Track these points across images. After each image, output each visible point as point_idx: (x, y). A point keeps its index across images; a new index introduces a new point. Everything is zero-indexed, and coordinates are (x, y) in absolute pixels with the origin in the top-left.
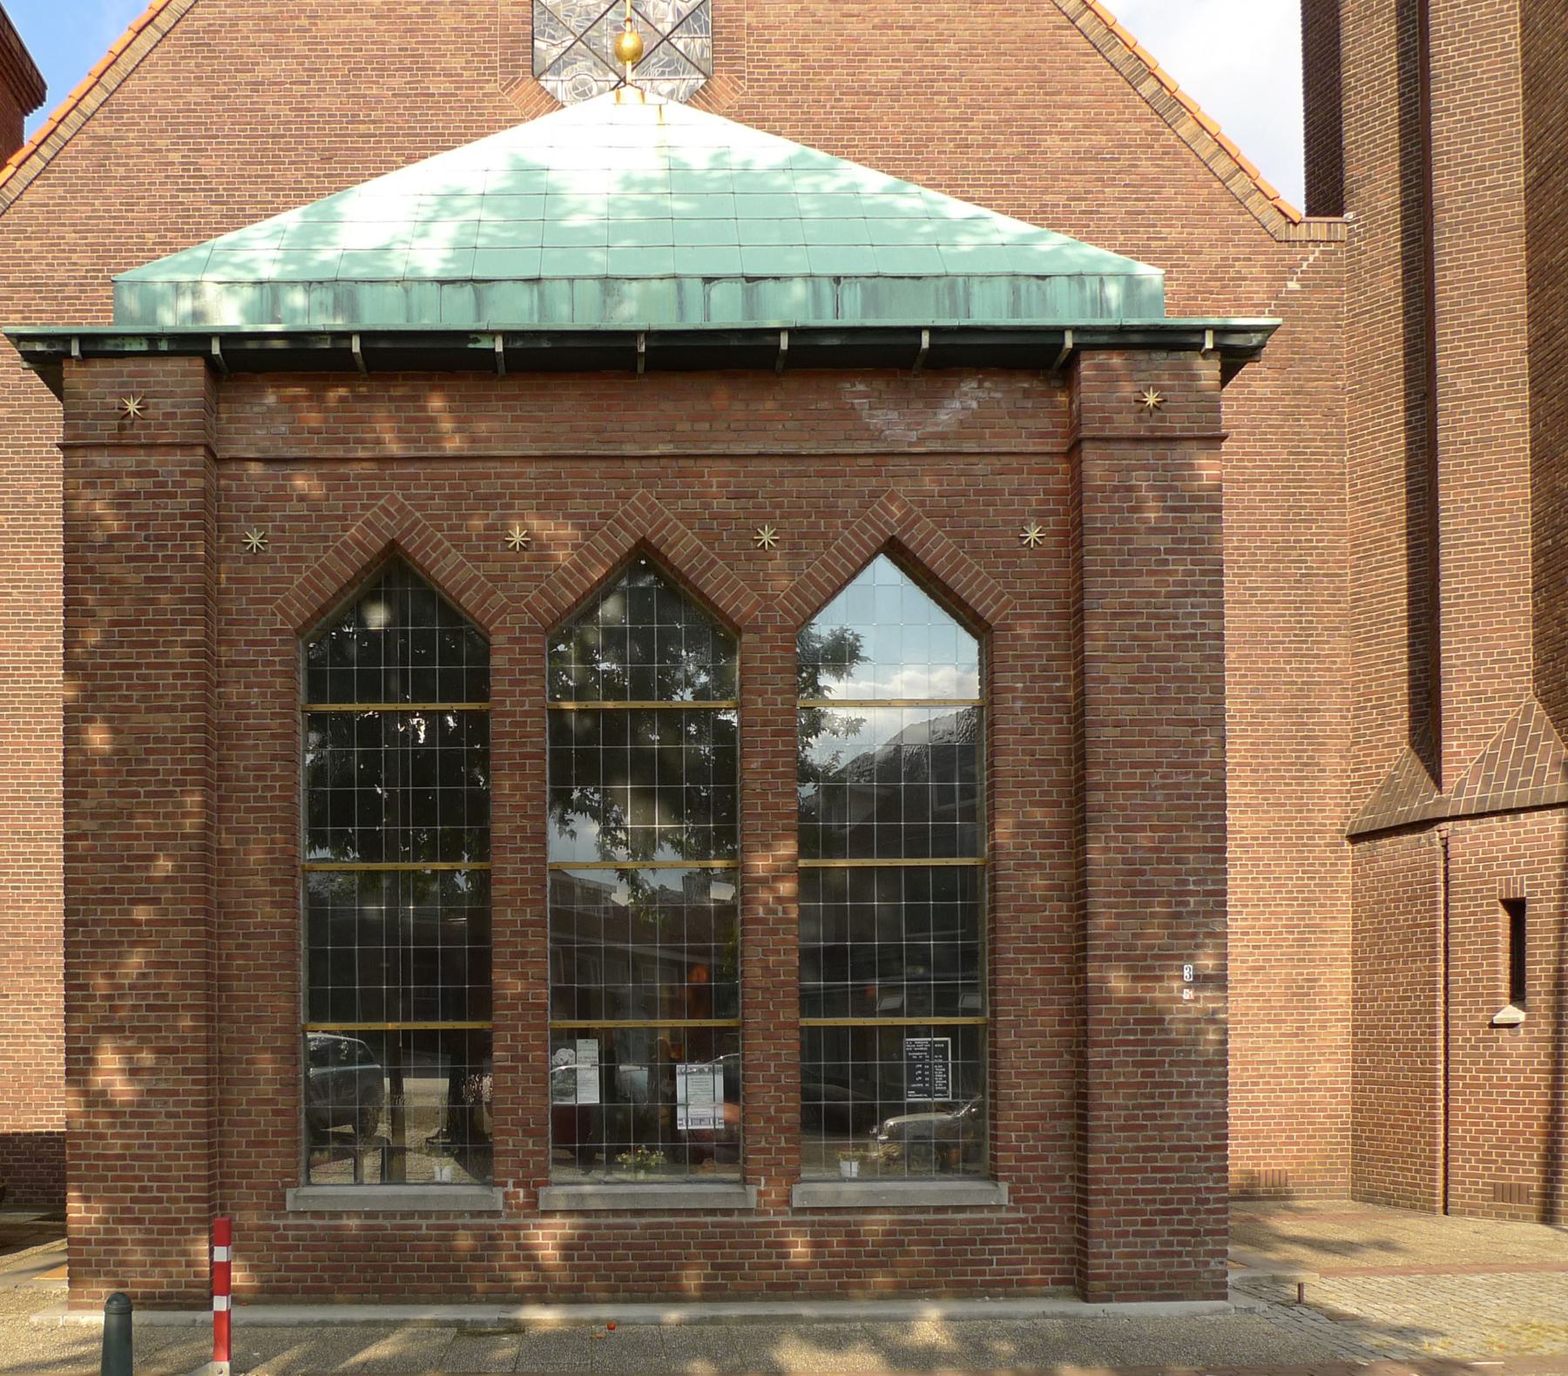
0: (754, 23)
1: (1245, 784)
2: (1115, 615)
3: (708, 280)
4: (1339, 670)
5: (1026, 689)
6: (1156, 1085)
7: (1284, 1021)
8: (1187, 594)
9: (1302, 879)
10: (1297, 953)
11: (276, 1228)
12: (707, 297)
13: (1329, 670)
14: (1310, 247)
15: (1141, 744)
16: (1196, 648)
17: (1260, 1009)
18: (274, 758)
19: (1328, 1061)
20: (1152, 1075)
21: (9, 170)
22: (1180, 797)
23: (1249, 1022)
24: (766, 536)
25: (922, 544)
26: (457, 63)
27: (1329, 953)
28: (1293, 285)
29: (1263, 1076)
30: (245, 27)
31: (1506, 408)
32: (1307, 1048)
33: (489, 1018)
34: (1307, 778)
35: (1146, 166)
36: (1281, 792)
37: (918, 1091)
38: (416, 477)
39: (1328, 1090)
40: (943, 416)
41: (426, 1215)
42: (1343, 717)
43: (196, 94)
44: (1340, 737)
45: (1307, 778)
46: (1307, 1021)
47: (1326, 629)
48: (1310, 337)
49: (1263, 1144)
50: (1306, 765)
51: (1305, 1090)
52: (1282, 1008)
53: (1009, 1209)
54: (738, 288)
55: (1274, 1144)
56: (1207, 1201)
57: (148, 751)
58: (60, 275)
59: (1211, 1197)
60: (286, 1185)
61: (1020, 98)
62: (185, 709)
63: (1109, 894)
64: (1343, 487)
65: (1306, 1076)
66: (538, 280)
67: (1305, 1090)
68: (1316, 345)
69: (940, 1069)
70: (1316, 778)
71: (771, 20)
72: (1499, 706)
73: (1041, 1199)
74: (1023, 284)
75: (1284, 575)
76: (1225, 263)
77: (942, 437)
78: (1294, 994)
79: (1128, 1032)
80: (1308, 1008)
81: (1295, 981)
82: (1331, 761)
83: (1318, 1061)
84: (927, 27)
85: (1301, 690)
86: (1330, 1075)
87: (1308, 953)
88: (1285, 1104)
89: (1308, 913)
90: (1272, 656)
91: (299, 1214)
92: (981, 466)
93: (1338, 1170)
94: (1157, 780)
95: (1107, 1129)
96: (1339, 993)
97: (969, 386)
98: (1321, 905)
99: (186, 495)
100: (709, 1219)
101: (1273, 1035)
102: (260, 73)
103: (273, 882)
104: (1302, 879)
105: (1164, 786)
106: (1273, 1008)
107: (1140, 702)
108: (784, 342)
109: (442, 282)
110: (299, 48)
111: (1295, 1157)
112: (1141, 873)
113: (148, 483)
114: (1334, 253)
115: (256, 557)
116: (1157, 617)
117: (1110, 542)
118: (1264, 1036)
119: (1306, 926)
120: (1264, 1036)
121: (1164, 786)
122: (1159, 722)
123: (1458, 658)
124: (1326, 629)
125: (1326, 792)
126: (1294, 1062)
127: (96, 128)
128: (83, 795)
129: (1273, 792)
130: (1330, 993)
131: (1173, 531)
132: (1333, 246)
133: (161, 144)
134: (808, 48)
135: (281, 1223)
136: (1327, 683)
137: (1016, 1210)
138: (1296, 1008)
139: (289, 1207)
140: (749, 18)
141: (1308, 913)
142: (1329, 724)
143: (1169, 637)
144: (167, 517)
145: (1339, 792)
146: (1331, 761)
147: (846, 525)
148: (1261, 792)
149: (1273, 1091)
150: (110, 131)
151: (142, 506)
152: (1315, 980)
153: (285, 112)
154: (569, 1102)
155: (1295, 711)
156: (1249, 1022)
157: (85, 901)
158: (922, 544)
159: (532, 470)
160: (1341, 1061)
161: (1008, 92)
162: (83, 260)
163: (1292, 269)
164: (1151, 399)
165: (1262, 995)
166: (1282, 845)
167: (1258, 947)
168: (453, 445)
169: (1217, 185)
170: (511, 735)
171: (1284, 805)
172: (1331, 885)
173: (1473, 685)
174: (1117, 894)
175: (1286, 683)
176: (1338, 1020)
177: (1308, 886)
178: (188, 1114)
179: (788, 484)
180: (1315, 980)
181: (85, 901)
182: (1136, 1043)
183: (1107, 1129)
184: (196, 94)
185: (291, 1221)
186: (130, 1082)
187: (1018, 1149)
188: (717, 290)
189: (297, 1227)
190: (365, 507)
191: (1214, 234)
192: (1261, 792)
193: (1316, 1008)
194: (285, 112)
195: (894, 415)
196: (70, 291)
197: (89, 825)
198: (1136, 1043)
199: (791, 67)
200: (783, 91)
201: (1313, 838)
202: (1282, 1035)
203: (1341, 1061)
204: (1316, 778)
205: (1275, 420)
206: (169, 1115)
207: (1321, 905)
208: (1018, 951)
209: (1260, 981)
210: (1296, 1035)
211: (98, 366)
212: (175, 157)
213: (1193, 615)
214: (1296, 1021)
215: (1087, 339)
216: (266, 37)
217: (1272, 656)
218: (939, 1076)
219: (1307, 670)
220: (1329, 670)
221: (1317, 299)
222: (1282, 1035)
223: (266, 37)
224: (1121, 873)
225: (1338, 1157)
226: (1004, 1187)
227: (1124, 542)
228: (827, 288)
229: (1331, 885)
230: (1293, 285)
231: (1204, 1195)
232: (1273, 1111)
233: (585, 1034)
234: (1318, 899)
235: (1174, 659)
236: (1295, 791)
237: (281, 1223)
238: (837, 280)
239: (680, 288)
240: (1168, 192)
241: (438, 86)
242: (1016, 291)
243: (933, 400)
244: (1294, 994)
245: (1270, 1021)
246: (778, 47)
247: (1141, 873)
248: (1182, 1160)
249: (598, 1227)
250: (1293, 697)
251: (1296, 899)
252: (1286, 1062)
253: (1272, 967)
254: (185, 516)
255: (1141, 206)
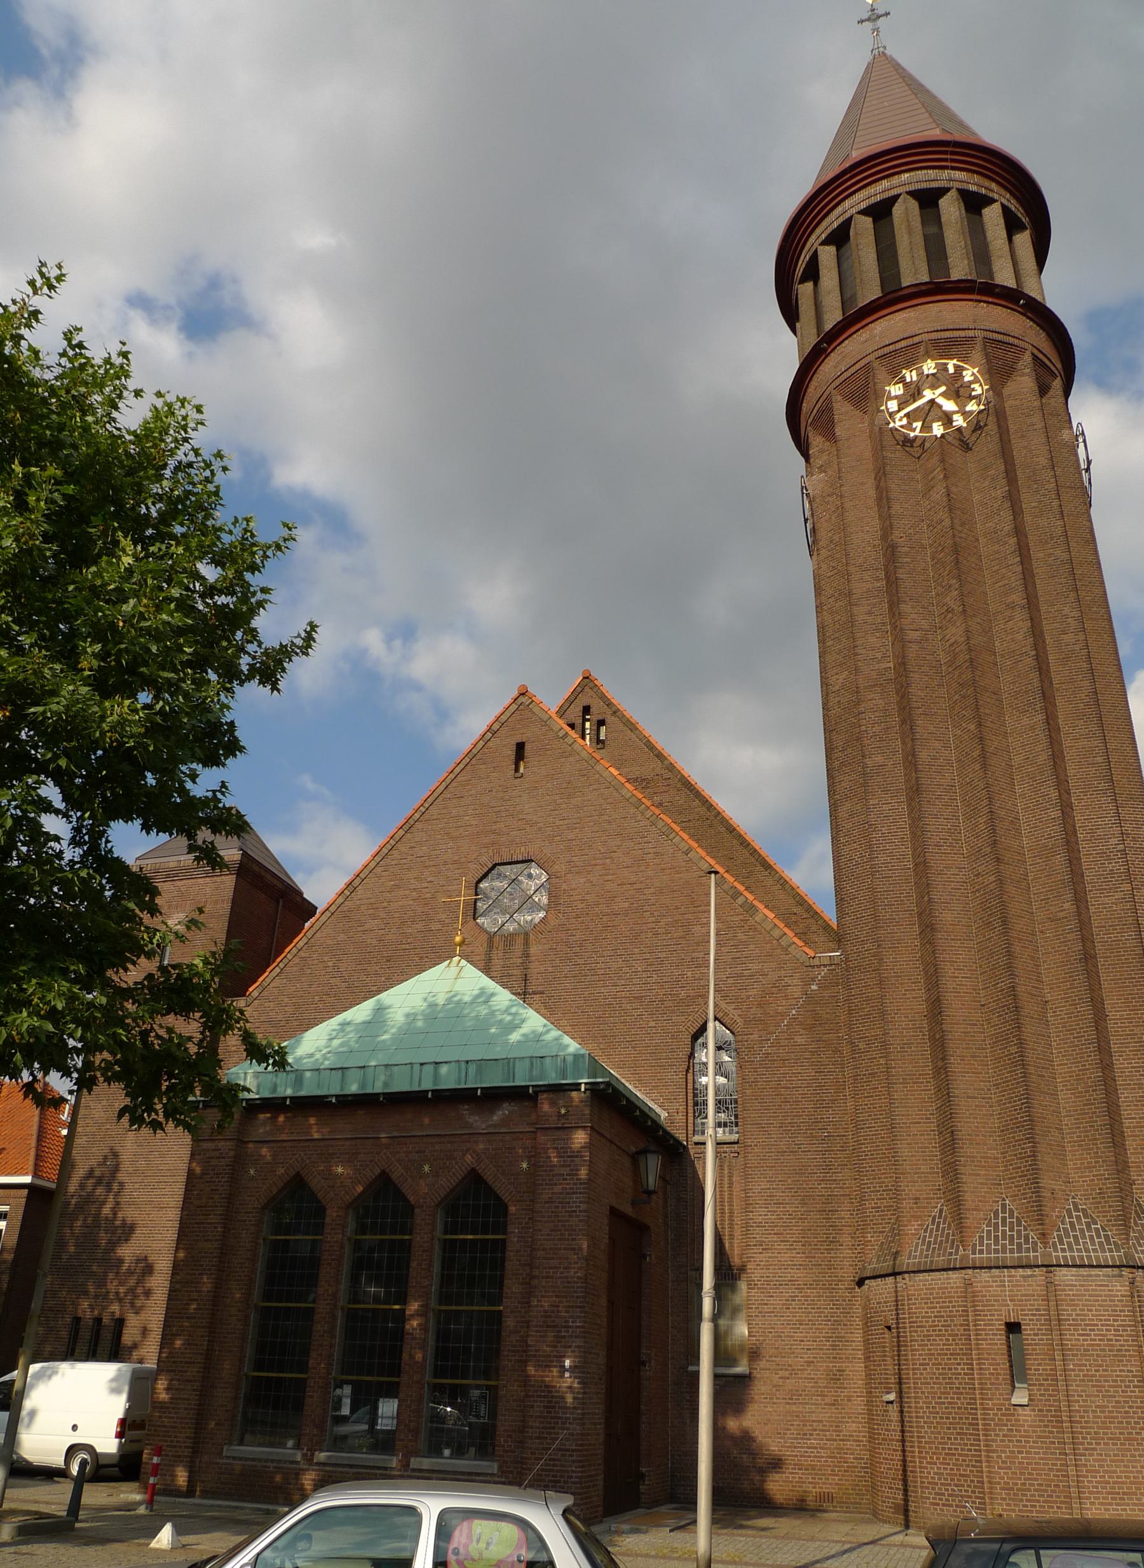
0: (566, 888)
1: (799, 1253)
2: (546, 1202)
3: (422, 1064)
4: (847, 1188)
5: (519, 1232)
6: (552, 1418)
7: (827, 1396)
8: (574, 1193)
9: (832, 1309)
10: (831, 1354)
11: (218, 1464)
12: (421, 1071)
13: (842, 1188)
14: (822, 968)
15: (553, 1258)
16: (576, 1216)
17: (812, 1387)
18: (247, 1259)
19: (853, 1422)
20: (550, 1412)
21: (267, 974)
22: (568, 1282)
23: (806, 1395)
24: (426, 1168)
25: (484, 1170)
26: (443, 916)
27: (851, 1354)
28: (814, 987)
29: (815, 1430)
30: (363, 908)
31: (880, 1057)
32: (841, 1413)
33: (399, 1376)
34: (832, 1249)
35: (741, 936)
36: (819, 1257)
37: (474, 1416)
38: (309, 1146)
39: (854, 1441)
40: (495, 1118)
41: (273, 1461)
42: (852, 1214)
43: (342, 937)
44: (850, 1226)
45: (832, 1249)
46: (840, 1396)
47: (839, 1165)
48: (824, 1012)
49: (816, 1474)
50: (832, 1242)
51: (841, 1440)
52: (824, 1387)
53: (498, 1476)
54: (432, 1067)
55: (824, 1475)
56: (572, 1477)
57: (202, 1257)
58: (280, 1017)
59: (574, 1475)
60: (225, 1444)
61: (683, 910)
62: (216, 1240)
63: (536, 1326)
64: (845, 1089)
65: (841, 1431)
66: (364, 1067)
67: (841, 1440)
68: (828, 1016)
69: (483, 1406)
70: (837, 1249)
71: (573, 886)
72: (887, 1215)
73: (512, 1473)
74: (534, 1060)
75: (815, 1137)
76: (780, 979)
77: (494, 1126)
78: (832, 1379)
79: (541, 1391)
80: (840, 1388)
81: (831, 1371)
82: (846, 1240)
83: (848, 1422)
84: (641, 882)
85: (827, 1199)
86: (855, 1431)
87: (838, 1354)
88: (829, 1449)
89: (837, 1329)
90: (810, 1181)
91: (228, 1457)
92: (508, 1138)
93: (863, 1495)
94: (558, 1275)
95: (531, 1438)
96: (858, 1380)
97: (505, 1105)
98: (845, 1325)
99: (228, 1158)
100: (378, 1472)
101: (820, 1404)
102: (367, 927)
103: (239, 1311)
104: (832, 1309)
105: (561, 1278)
106: (820, 1387)
107: (553, 1240)
108: (430, 1095)
109: (332, 1069)
110: (382, 915)
111: (837, 1484)
112: (550, 1317)
113: (216, 1154)
114: (835, 970)
115: (252, 1178)
116: (562, 1203)
117: (546, 1171)
118: (815, 1404)
119: (837, 1337)
120: (815, 1404)
121: (561, 1278)
122: (560, 1249)
123: (868, 1188)
124: (839, 1165)
125: (843, 1257)
126: (833, 1421)
127: (302, 954)
128: (178, 1274)
129: (814, 1257)
130: (853, 1379)
131: (570, 1166)
132: (833, 967)
133: (326, 959)
134: (588, 897)
135: (221, 1461)
136: (841, 1195)
137: (502, 1477)
138: (833, 1388)
139: (224, 1454)
140: (564, 886)
141: (837, 1329)
142: (843, 1218)
143: (566, 1212)
144: (222, 1166)
145: (851, 1257)
146: (846, 1240)
147: (457, 1163)
148: (807, 1257)
149: (822, 1440)
150: (307, 955)
151: (214, 1162)
152: (844, 1371)
153: (374, 942)
154: (338, 1413)
155: (825, 1211)
156: (806, 1395)
157: (171, 1317)
158: (484, 1170)
159: (348, 1143)
160: (861, 1423)
161: (677, 908)
162: (289, 1009)
163: (813, 979)
164: (563, 1111)
165: (813, 1379)
166: (820, 1288)
167: (809, 1349)
168: (316, 1136)
169: (774, 942)
170: (329, 1250)
171: (821, 1265)
172: (849, 1313)
173: (875, 1203)
174: (540, 1326)
175: (818, 1196)
176: (858, 1396)
177: (836, 1313)
178: (191, 1409)
179: (437, 1147)
180: (844, 1371)
181: (171, 1317)
182: (544, 1397)
183: (531, 1438)
184: (342, 937)
185: (225, 1461)
186: (167, 1394)
187: (504, 1446)
188: (425, 1067)
189: (226, 1464)
190: (290, 1159)
191: (773, 965)
192: (807, 1257)
193: (845, 1388)
194: (374, 942)
195: (477, 1118)
196: (282, 1023)
197: (178, 1286)
198: (544, 1397)
199: (581, 906)
200: (577, 917)
201: (838, 1285)
202: (825, 1404)
203: (861, 1423)
204: (837, 1249)
205: (807, 1054)
206: (185, 1409)
207: (845, 1325)
208: (509, 1351)
209: (811, 1370)
210: (834, 1405)
211: (209, 1111)
212: (330, 964)
213: (576, 1202)
214: (834, 1396)
215: (538, 1089)
216: (371, 911)
217: (810, 1181)
218: (483, 1408)
219: (830, 1188)
220: (842, 1188)
221: (826, 993)
222: (825, 1404)
223: (371, 911)
224: (542, 1316)
225: (863, 1486)
226: (496, 1465)
227: (550, 1171)
228: (463, 1065)
229: (849, 1313)
230: (814, 987)
231: (570, 1474)
232: (823, 1453)
233: (347, 1382)
234: (842, 1321)
235: (568, 1221)
236: (826, 1257)
237: (221, 1461)
238: (467, 1062)
239: (412, 1068)
240: (752, 947)
241: (435, 926)
242: (532, 1064)
243: (492, 1112)
244: (832, 1379)
245: (818, 1395)
246: (576, 898)
247: (550, 1317)
248: (562, 1455)
249: (335, 1472)
250: (823, 1203)
251: (830, 1321)
252: (829, 1422)
253: (818, 1362)
254: (227, 1166)
255: (738, 955)
